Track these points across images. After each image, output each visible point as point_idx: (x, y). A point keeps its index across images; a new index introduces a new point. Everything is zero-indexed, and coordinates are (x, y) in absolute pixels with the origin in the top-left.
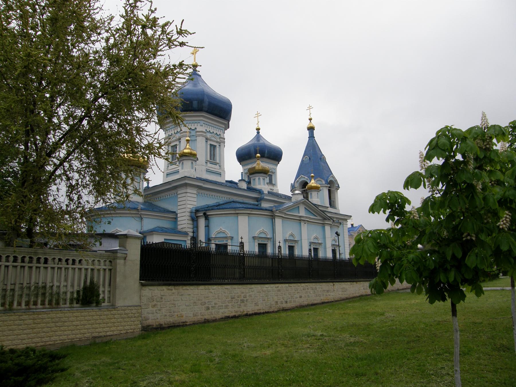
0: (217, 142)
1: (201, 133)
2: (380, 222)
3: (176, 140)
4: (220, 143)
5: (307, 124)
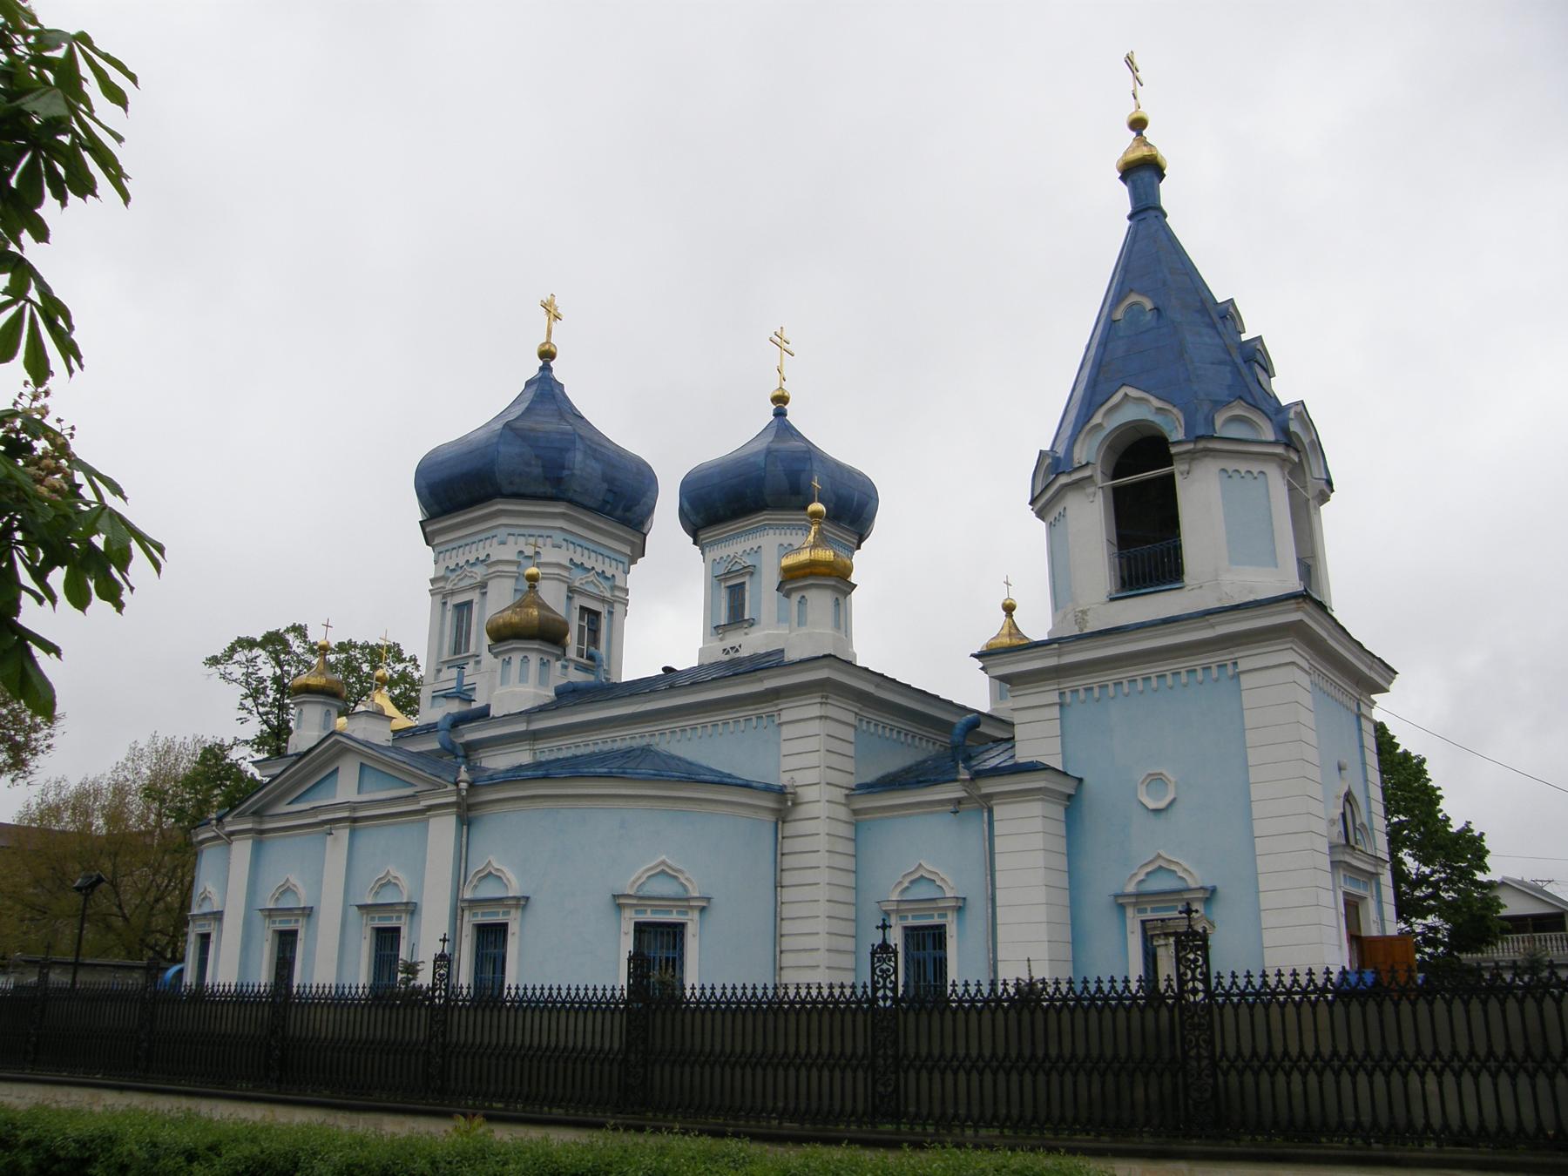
0: (603, 600)
1: (556, 571)
2: (427, 1169)
3: (472, 588)
4: (611, 604)
5: (1122, 144)
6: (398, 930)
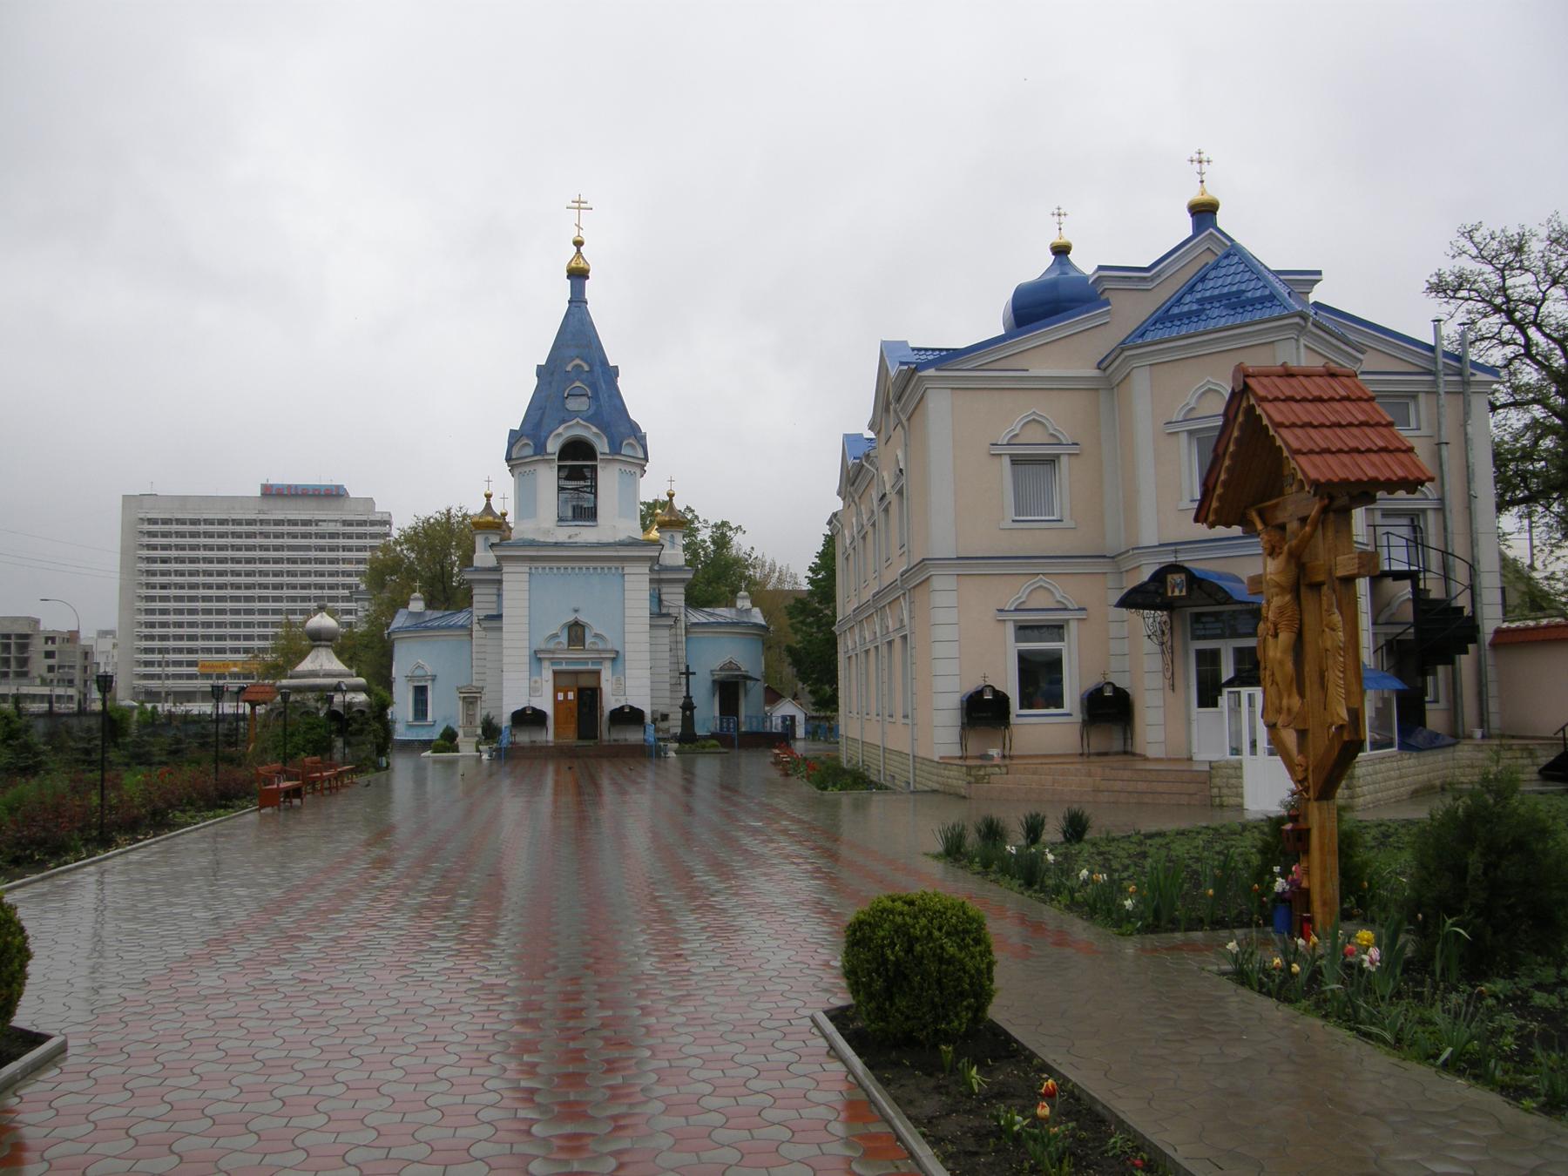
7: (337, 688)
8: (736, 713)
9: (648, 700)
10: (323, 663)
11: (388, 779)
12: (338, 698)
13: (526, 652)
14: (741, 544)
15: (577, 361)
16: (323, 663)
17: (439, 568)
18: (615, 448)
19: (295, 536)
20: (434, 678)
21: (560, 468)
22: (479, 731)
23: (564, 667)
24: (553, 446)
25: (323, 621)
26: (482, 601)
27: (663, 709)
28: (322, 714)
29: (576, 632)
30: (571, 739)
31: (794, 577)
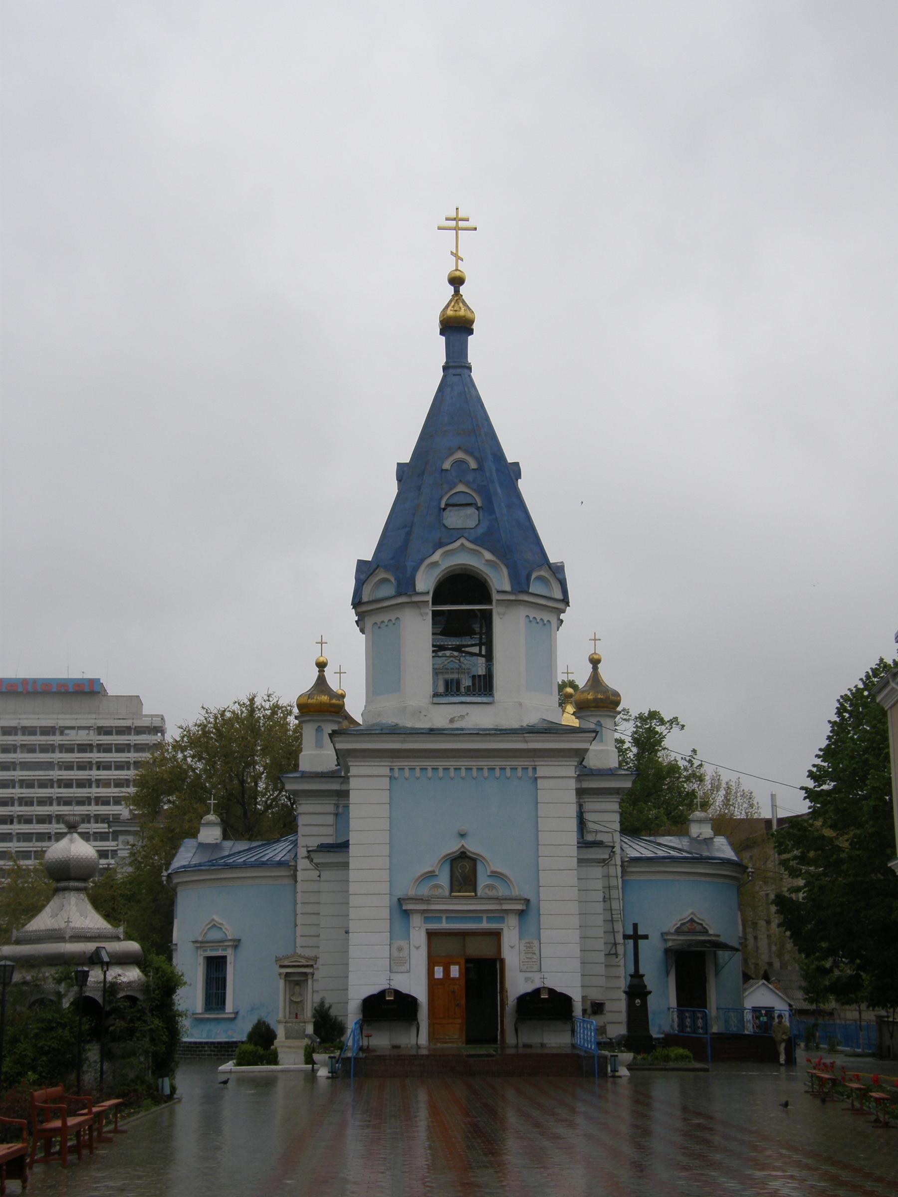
6: (224, 958)
7: (95, 959)
8: (702, 1002)
9: (577, 981)
10: (75, 917)
11: (172, 1114)
12: (95, 975)
13: (386, 901)
14: (675, 747)
15: (460, 455)
16: (75, 917)
17: (245, 781)
18: (520, 584)
19: (31, 749)
20: (236, 944)
21: (435, 614)
22: (310, 1029)
23: (444, 925)
24: (425, 582)
25: (78, 849)
26: (314, 823)
27: (596, 995)
28: (66, 1004)
29: (463, 869)
30: (455, 1042)
31: (749, 797)
